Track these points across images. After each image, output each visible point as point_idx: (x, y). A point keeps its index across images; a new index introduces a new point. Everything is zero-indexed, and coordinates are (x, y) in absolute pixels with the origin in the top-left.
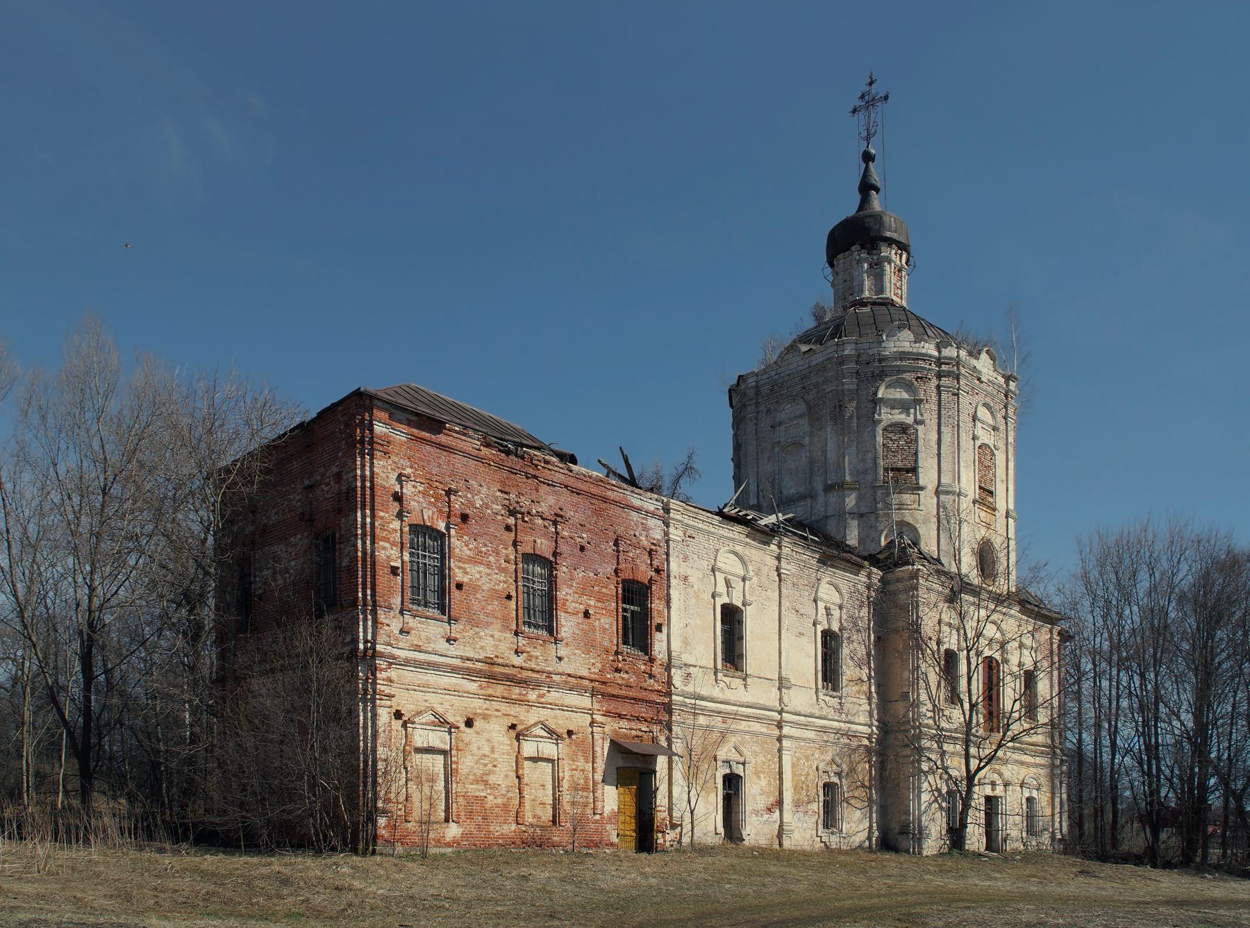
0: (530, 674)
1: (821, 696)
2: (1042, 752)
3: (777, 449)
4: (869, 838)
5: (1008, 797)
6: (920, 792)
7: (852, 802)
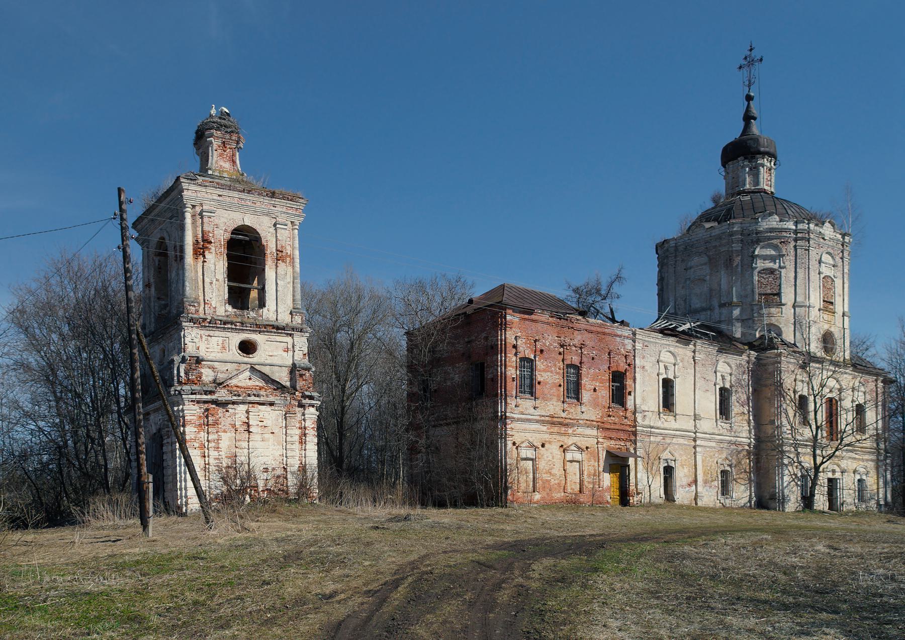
0: (569, 421)
1: (719, 423)
2: (869, 452)
3: (688, 282)
4: (750, 501)
5: (844, 480)
6: (783, 475)
7: (739, 481)
